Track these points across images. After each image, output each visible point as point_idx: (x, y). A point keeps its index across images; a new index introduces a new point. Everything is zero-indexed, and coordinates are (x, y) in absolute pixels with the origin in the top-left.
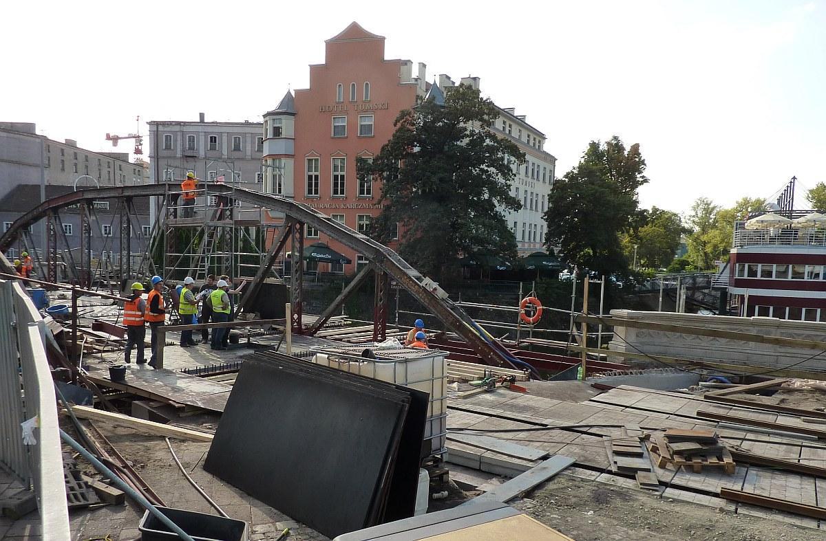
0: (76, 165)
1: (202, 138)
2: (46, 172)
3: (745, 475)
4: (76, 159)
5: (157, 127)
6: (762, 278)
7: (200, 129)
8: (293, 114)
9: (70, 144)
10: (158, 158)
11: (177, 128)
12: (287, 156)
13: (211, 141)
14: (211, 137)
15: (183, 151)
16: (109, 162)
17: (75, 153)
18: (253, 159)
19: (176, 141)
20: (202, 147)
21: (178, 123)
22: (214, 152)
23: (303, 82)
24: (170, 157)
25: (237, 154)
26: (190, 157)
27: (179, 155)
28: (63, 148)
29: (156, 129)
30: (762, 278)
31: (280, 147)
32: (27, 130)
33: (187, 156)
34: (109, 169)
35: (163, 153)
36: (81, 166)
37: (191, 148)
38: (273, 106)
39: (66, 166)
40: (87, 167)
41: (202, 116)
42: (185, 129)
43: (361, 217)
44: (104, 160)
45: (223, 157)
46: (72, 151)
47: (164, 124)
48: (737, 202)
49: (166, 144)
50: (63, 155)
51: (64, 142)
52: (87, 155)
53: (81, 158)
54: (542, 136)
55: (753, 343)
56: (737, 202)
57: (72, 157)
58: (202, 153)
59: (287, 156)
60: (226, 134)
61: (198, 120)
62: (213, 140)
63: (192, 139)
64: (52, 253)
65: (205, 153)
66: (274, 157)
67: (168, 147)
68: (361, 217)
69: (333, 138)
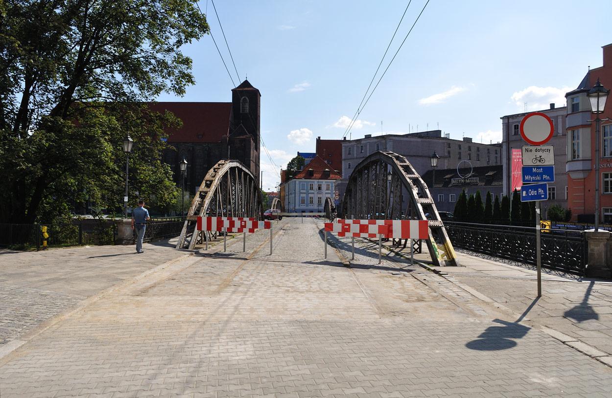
0: (470, 155)
3: (535, 307)
4: (470, 150)
6: (429, 195)
10: (509, 143)
13: (515, 129)
14: (515, 126)
16: (496, 150)
18: (357, 158)
22: (518, 136)
25: (350, 156)
28: (461, 144)
29: (507, 122)
30: (429, 195)
35: (512, 138)
36: (474, 155)
39: (462, 156)
41: (345, 138)
43: (606, 176)
45: (559, 135)
46: (468, 145)
50: (460, 149)
52: (479, 146)
53: (474, 149)
54: (439, 132)
60: (561, 117)
61: (343, 139)
67: (516, 133)
68: (606, 176)
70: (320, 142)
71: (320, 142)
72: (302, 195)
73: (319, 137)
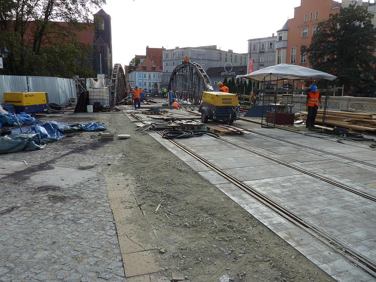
1: (267, 44)
2: (219, 62)
5: (251, 42)
7: (273, 40)
8: (287, 30)
9: (230, 51)
11: (258, 41)
12: (283, 48)
13: (270, 45)
15: (260, 50)
17: (231, 55)
19: (257, 46)
20: (266, 48)
21: (258, 39)
22: (255, 51)
23: (291, 15)
24: (255, 53)
26: (262, 52)
27: (258, 51)
31: (281, 45)
32: (214, 48)
33: (261, 52)
34: (245, 60)
37: (263, 49)
38: (281, 27)
40: (241, 60)
42: (261, 41)
44: (243, 56)
46: (230, 54)
47: (253, 40)
48: (163, 47)
49: (254, 48)
50: (226, 56)
51: (228, 51)
52: (236, 55)
53: (234, 56)
55: (9, 76)
56: (163, 47)
57: (230, 56)
58: (266, 50)
59: (283, 48)
62: (271, 44)
63: (263, 45)
64: (191, 88)
65: (268, 50)
66: (279, 49)
67: (254, 49)
69: (302, 38)
70: (148, 49)
71: (148, 49)
72: (139, 81)
73: (148, 46)
